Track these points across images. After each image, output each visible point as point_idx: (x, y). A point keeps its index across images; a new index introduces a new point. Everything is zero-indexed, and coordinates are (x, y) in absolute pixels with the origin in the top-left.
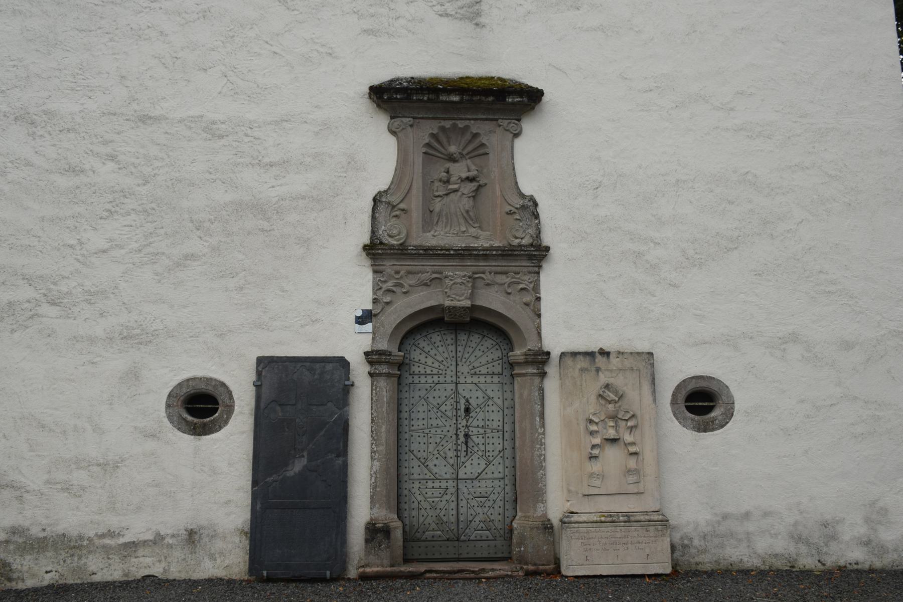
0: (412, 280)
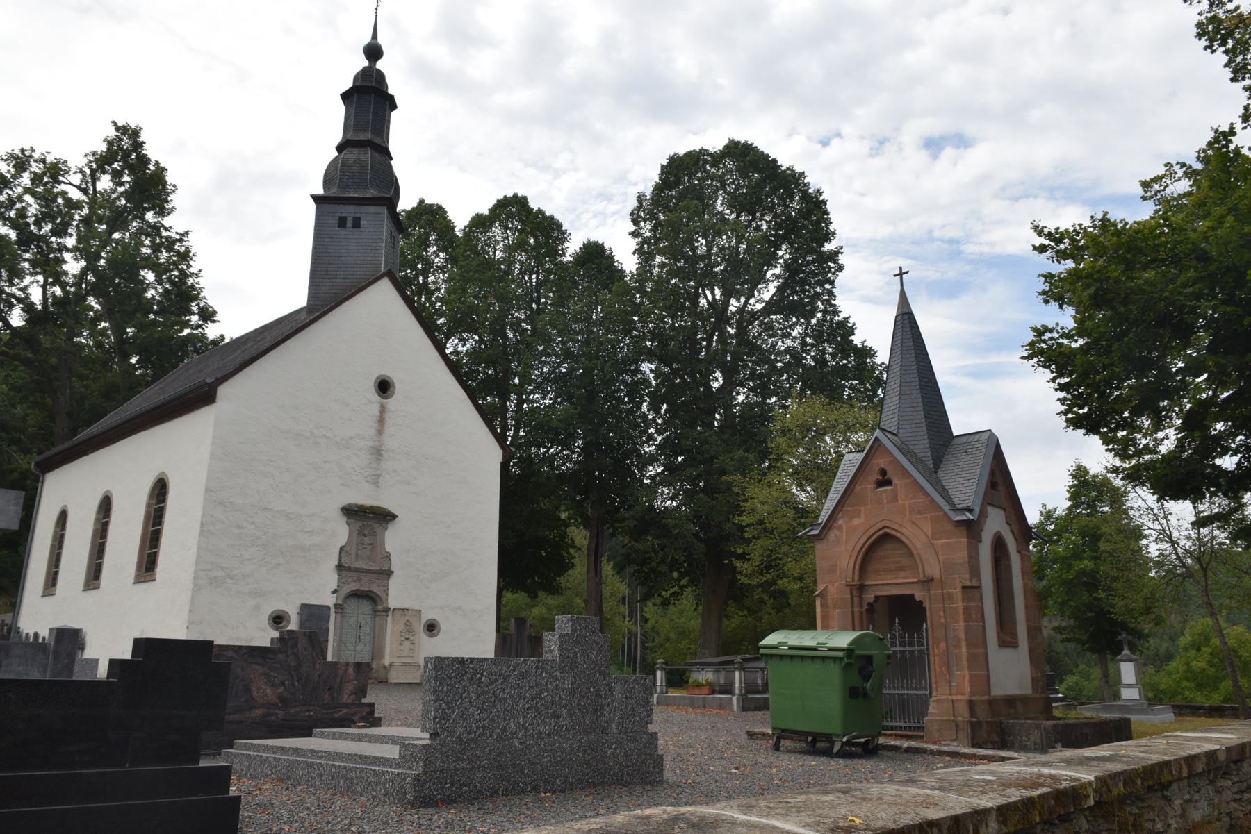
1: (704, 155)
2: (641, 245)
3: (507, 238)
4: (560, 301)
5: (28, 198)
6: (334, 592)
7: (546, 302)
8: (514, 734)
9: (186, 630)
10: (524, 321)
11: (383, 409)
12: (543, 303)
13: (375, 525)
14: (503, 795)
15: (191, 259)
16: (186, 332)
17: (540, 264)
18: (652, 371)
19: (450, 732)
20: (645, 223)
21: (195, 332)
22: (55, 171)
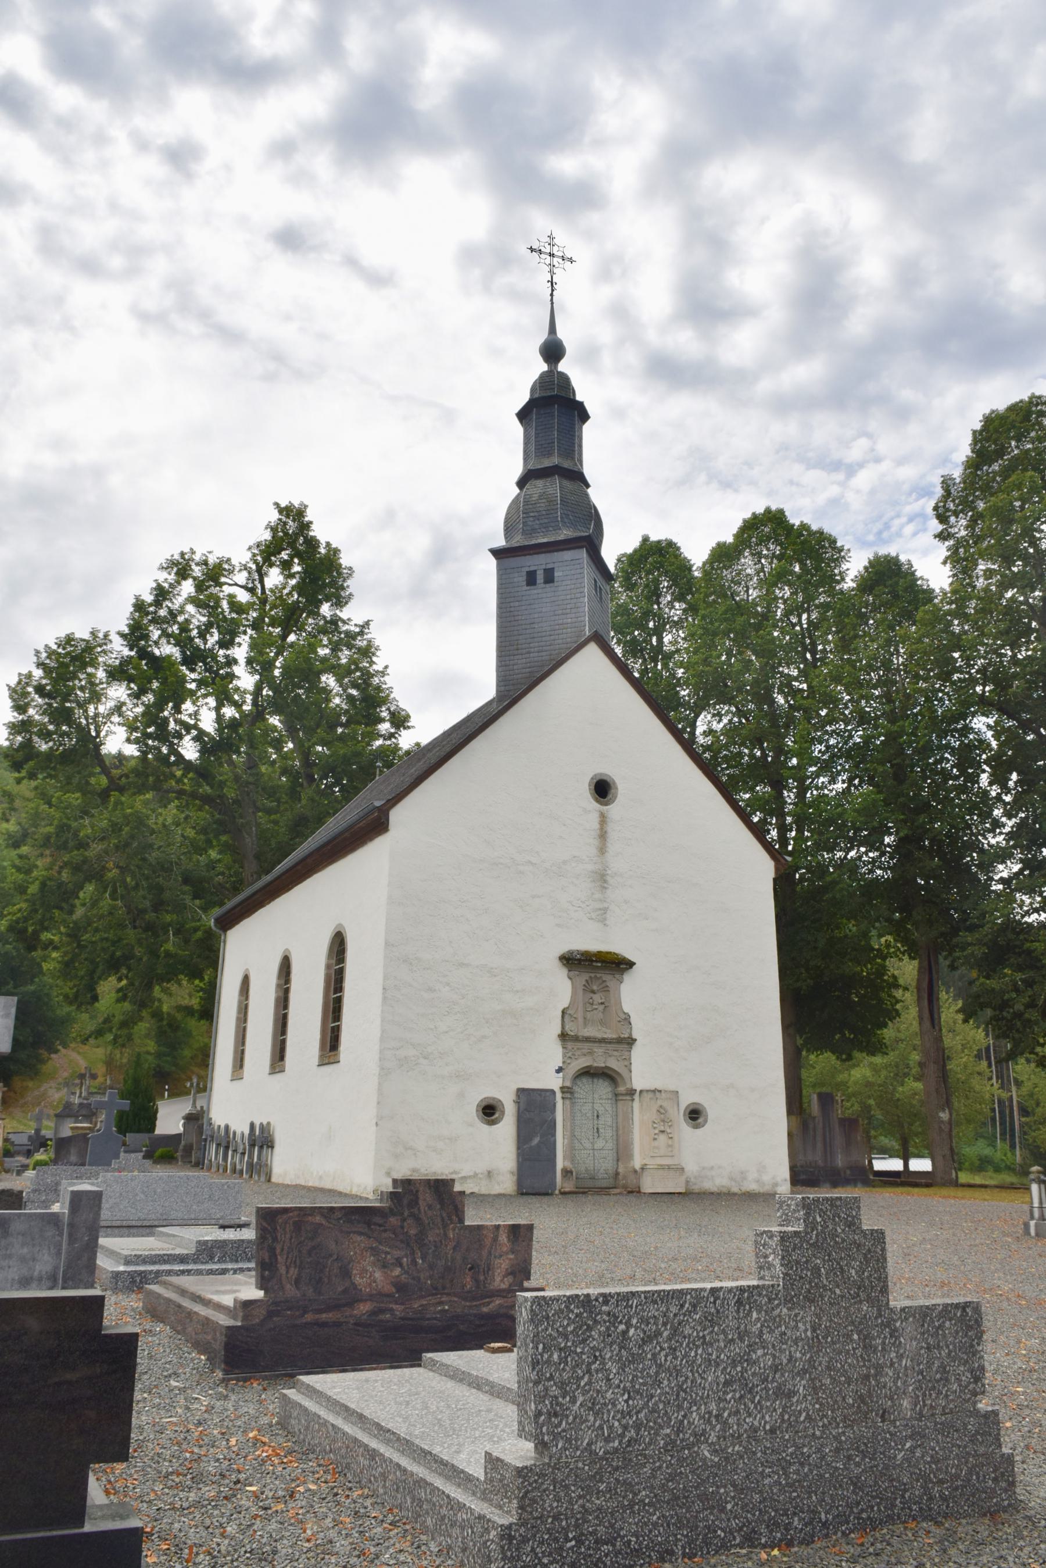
0: (578, 1053)
1: (1037, 404)
2: (954, 551)
3: (762, 570)
4: (845, 645)
5: (190, 608)
6: (559, 1070)
7: (825, 649)
8: (700, 1436)
9: (374, 1128)
10: (796, 679)
11: (603, 819)
12: (821, 651)
13: (607, 977)
14: (684, 1555)
15: (374, 654)
16: (379, 742)
17: (809, 599)
18: (989, 726)
19: (569, 1440)
20: (957, 517)
21: (388, 742)
22: (215, 573)
